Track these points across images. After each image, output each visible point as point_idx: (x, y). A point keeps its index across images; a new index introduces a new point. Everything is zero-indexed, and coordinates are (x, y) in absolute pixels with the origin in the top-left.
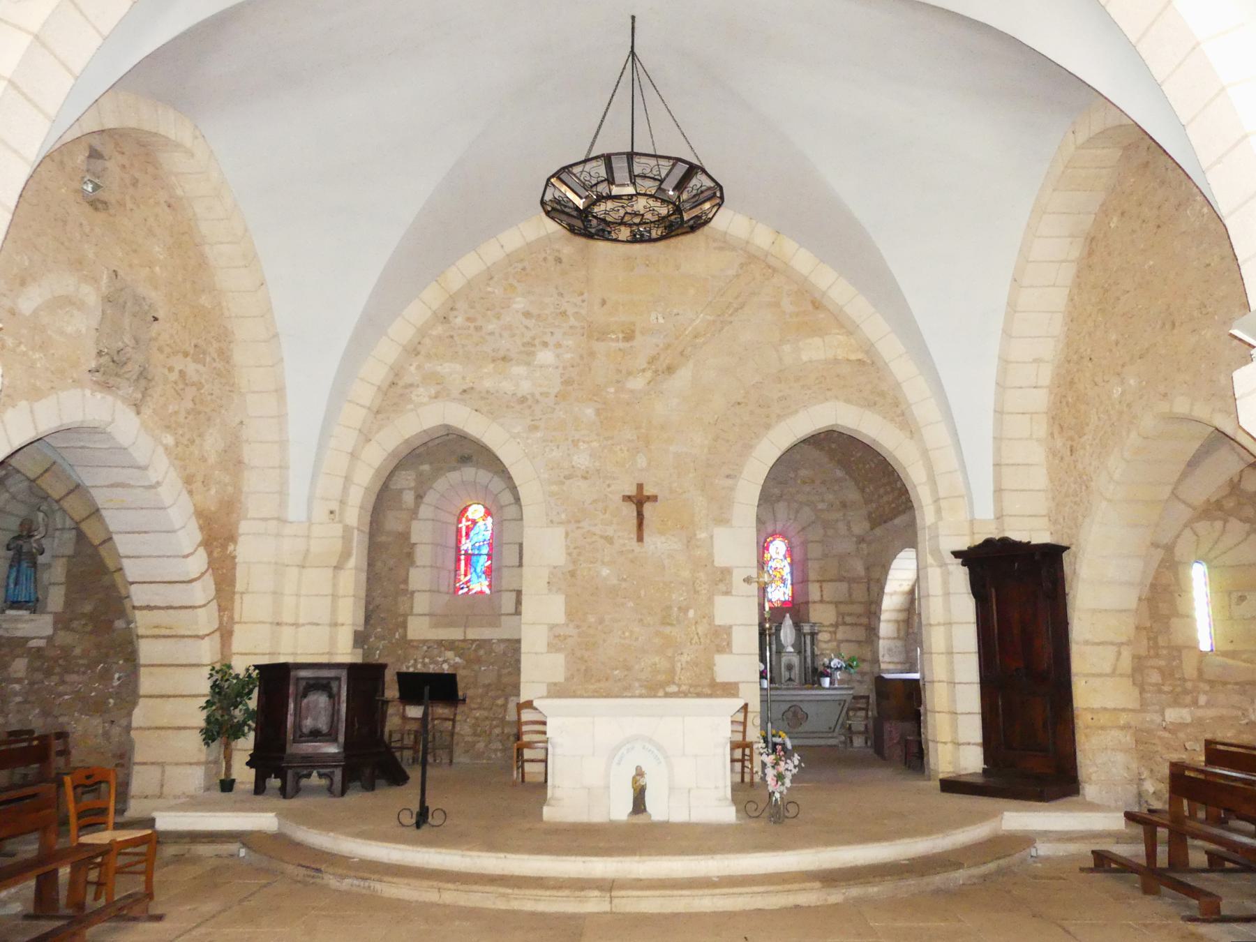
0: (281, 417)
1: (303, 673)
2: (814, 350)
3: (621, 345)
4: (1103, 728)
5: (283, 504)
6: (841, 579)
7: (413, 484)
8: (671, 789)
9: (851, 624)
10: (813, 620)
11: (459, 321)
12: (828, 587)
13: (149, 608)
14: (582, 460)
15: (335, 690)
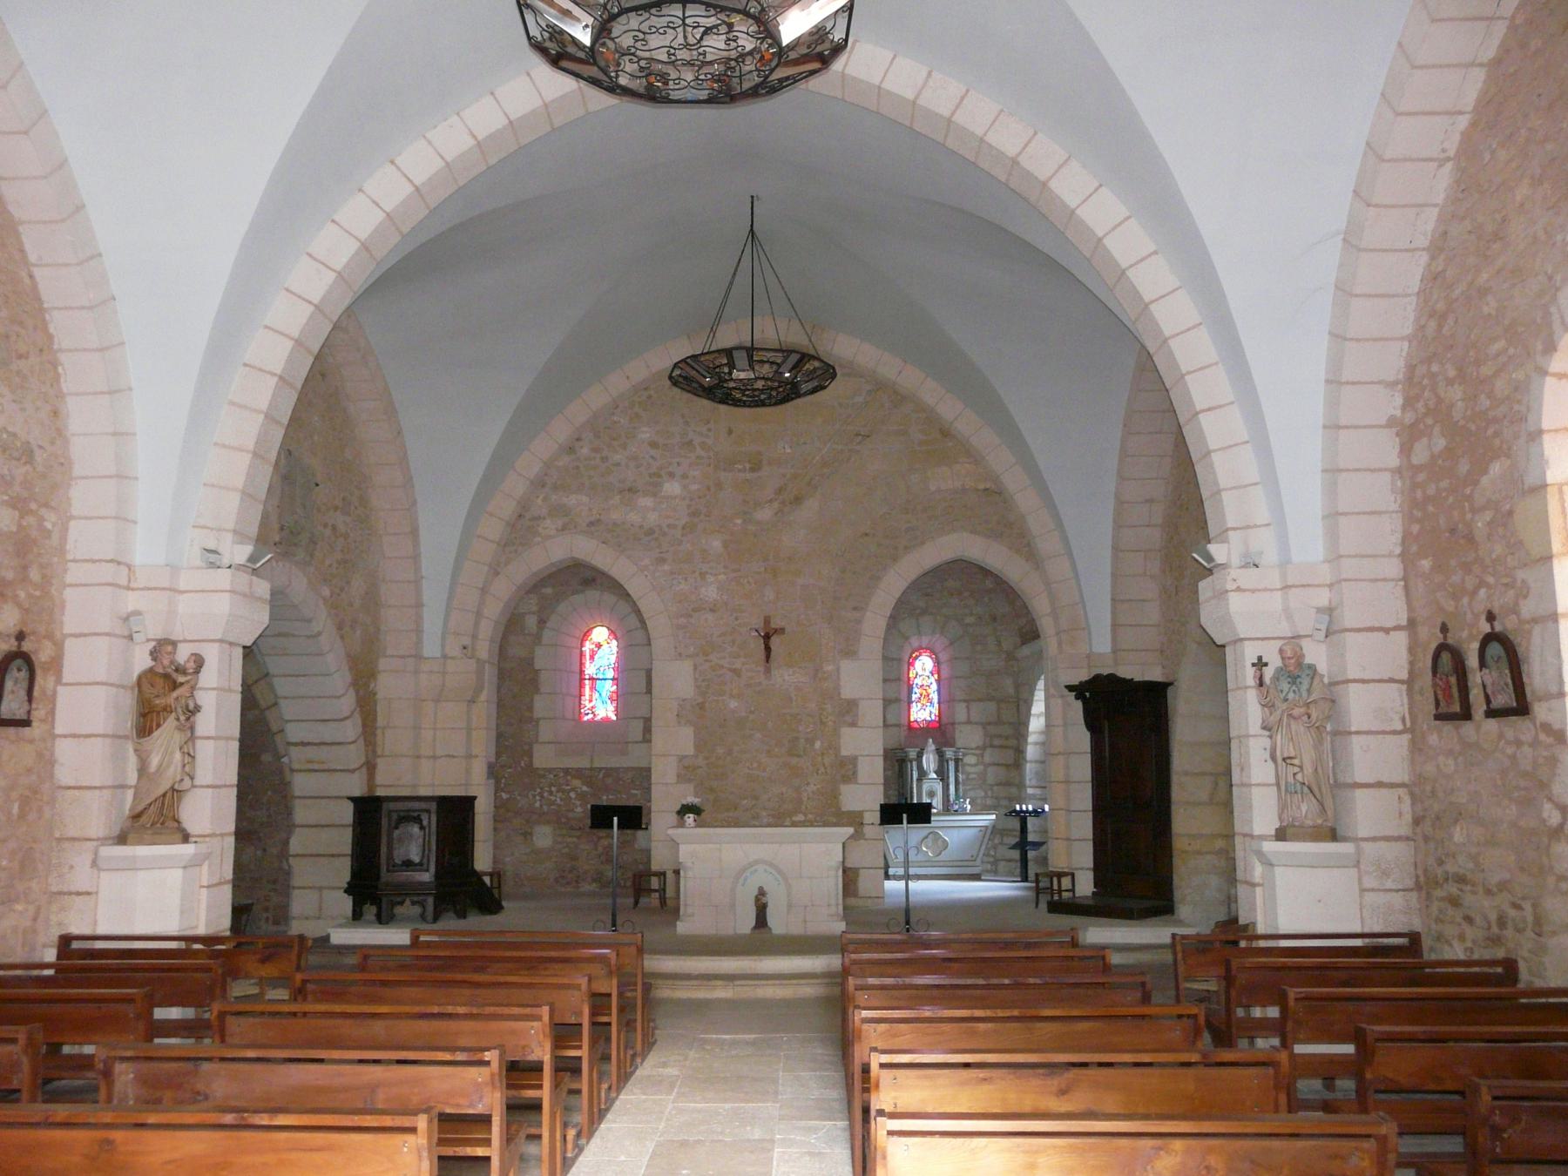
0: (416, 558)
1: (392, 806)
2: (944, 479)
3: (749, 476)
4: (1199, 853)
5: (419, 643)
6: (991, 699)
7: (535, 609)
8: (790, 906)
9: (1001, 747)
10: (959, 744)
11: (585, 451)
12: (975, 707)
13: (303, 744)
14: (710, 593)
15: (425, 823)
